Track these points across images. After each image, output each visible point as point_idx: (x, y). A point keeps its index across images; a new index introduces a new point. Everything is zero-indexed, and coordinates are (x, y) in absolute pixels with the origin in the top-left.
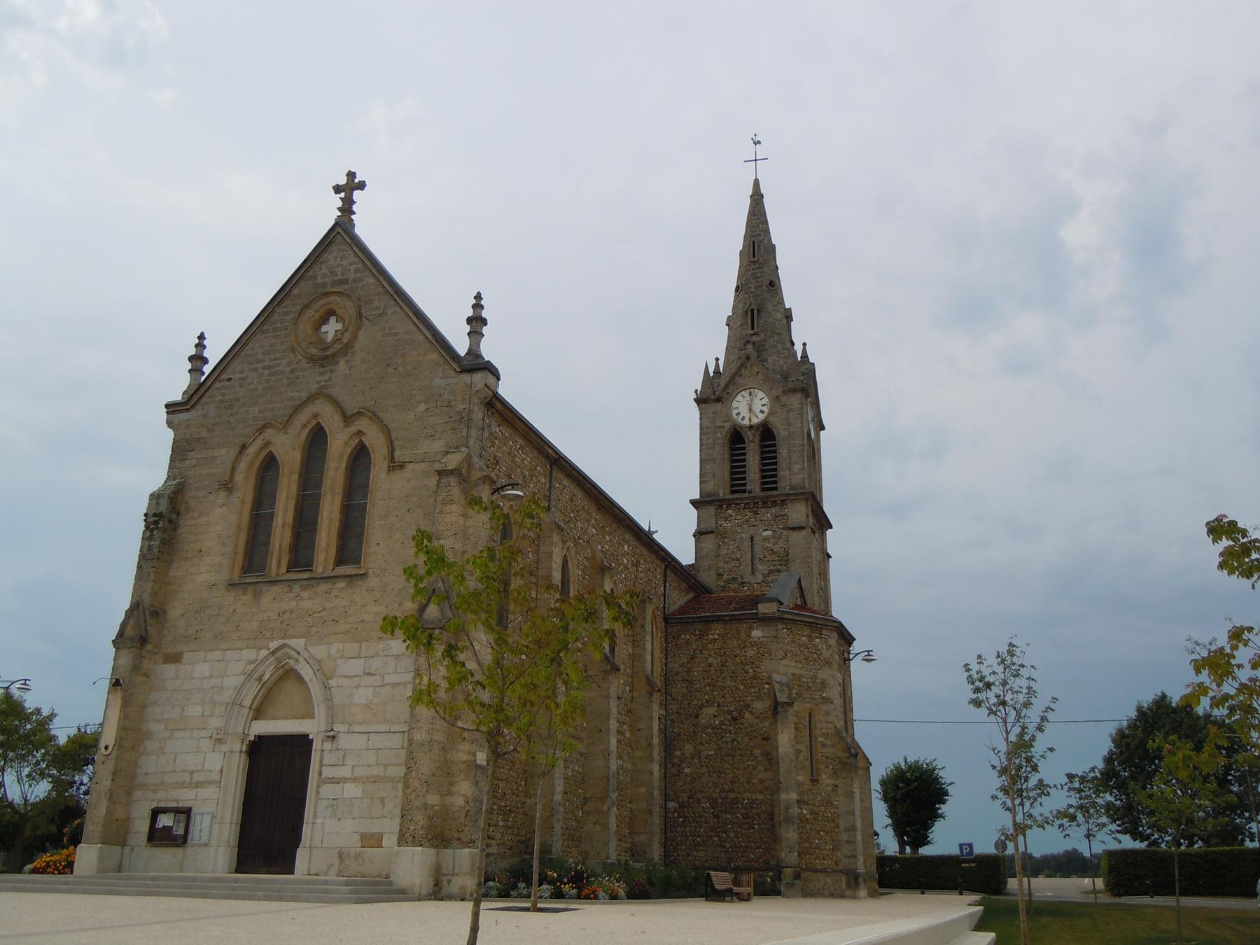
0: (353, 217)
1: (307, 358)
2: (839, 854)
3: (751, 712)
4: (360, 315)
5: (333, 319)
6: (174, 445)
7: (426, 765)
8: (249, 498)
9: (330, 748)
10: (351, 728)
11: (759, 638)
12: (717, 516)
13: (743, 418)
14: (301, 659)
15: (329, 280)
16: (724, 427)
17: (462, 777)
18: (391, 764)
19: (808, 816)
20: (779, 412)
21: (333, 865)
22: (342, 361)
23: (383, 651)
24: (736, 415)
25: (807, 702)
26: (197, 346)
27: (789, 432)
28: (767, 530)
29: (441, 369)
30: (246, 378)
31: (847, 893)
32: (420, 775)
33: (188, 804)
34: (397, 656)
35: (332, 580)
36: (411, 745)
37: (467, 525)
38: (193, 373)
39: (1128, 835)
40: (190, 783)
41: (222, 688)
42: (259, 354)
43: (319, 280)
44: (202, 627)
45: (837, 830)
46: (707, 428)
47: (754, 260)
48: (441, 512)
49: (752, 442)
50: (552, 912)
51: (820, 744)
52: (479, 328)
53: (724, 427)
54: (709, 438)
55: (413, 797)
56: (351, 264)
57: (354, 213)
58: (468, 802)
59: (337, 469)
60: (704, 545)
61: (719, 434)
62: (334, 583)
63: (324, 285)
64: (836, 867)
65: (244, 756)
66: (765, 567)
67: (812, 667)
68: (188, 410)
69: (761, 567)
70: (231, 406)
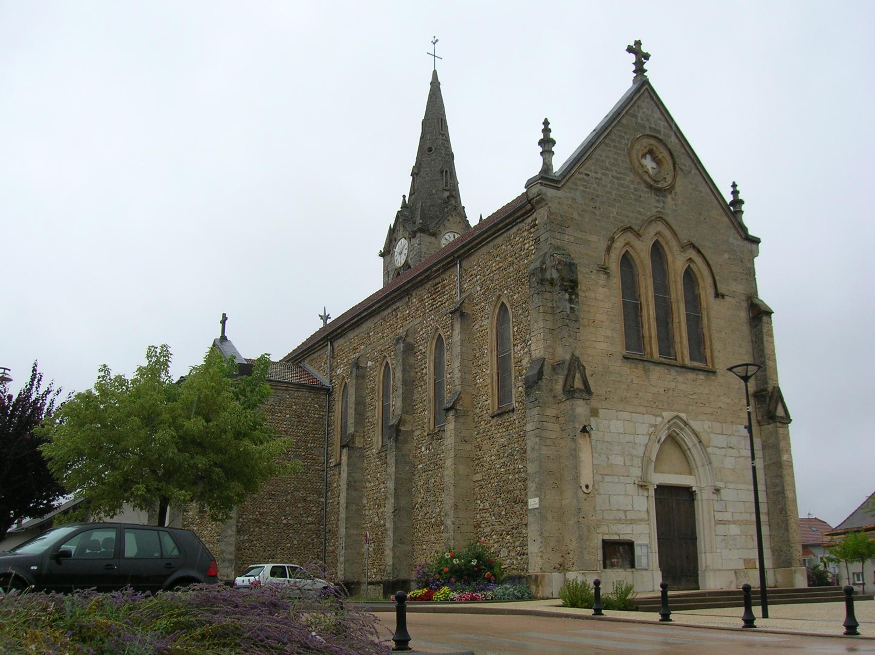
26: (541, 143)
35: (696, 372)
40: (626, 520)
41: (635, 443)
44: (609, 389)
57: (646, 71)
62: (697, 374)
68: (558, 188)
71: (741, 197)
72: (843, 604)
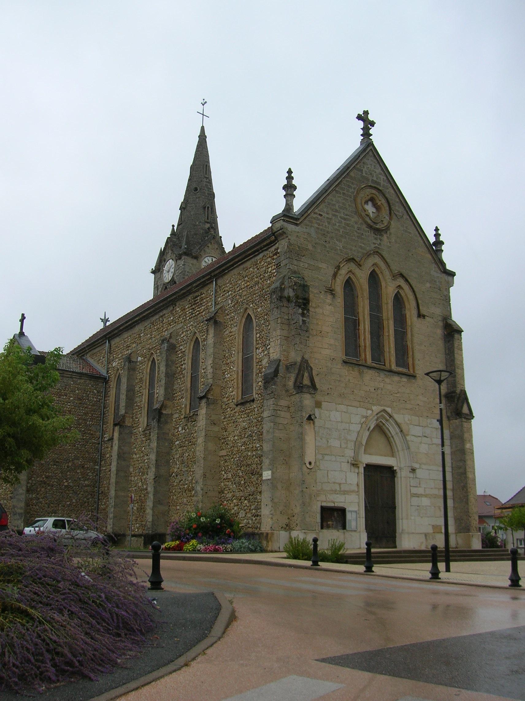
26: (435, 235)
39: (270, 225)
40: (340, 491)
62: (401, 378)
68: (297, 225)
72: (510, 563)
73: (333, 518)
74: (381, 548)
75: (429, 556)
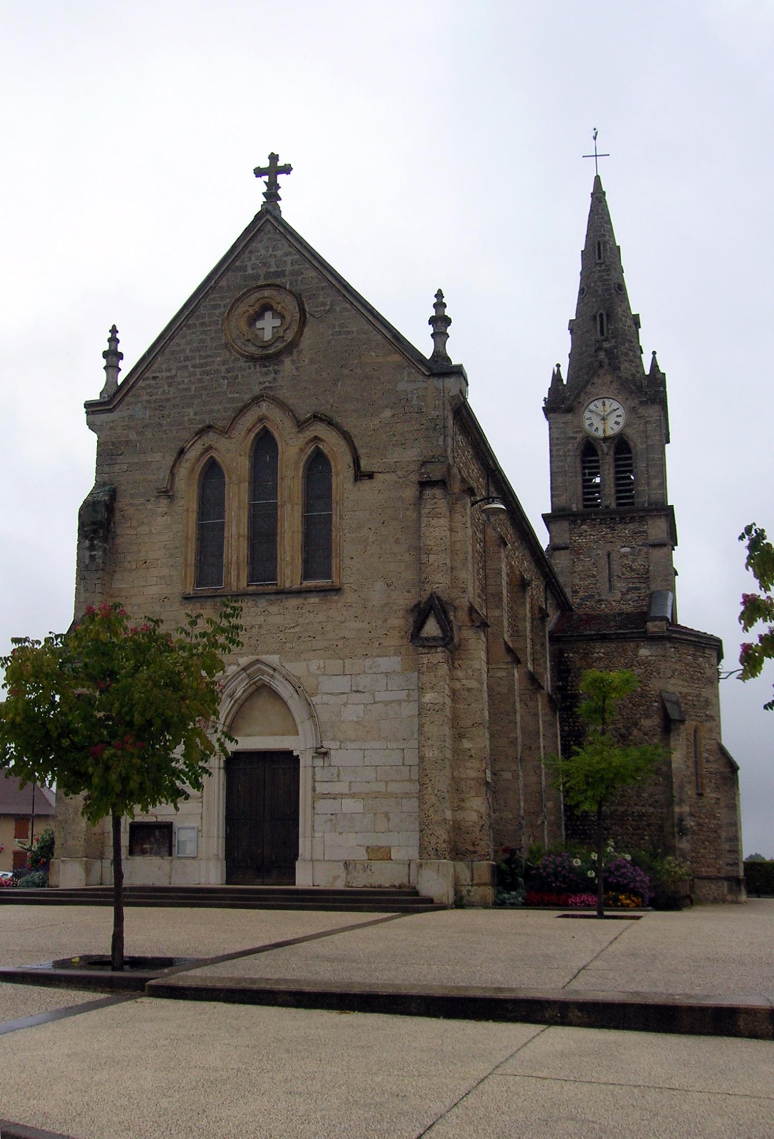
0: (279, 202)
1: (246, 357)
2: (721, 862)
3: (640, 729)
4: (302, 311)
5: (268, 315)
6: (100, 449)
7: (441, 781)
8: (194, 506)
9: (322, 765)
10: (343, 745)
11: (647, 657)
12: (571, 531)
13: (597, 429)
14: (276, 675)
15: (262, 272)
16: (576, 438)
17: (473, 794)
18: (392, 781)
19: (695, 828)
20: (635, 424)
21: (339, 876)
22: (287, 362)
23: (370, 668)
24: (589, 425)
25: (693, 720)
27: (648, 446)
28: (625, 546)
29: (406, 372)
30: (173, 377)
31: (729, 897)
32: (436, 792)
33: (168, 819)
34: (387, 674)
35: (304, 595)
36: (423, 762)
37: (454, 539)
38: (110, 370)
42: (188, 351)
43: (250, 271)
45: (720, 840)
46: (557, 439)
47: (599, 261)
48: (428, 525)
49: (607, 454)
50: (36, 904)
51: (705, 760)
52: (443, 328)
53: (576, 438)
54: (560, 449)
55: (431, 813)
56: (286, 255)
57: (280, 199)
58: (481, 817)
59: (294, 478)
60: (558, 561)
61: (570, 445)
62: (305, 599)
63: (256, 277)
64: (719, 875)
65: (222, 771)
66: (624, 585)
67: (697, 686)
68: (111, 411)
69: (620, 585)
70: (161, 408)
71: (447, 312)
72: (111, 909)
73: (152, 839)
74: (263, 885)
75: (126, 896)
